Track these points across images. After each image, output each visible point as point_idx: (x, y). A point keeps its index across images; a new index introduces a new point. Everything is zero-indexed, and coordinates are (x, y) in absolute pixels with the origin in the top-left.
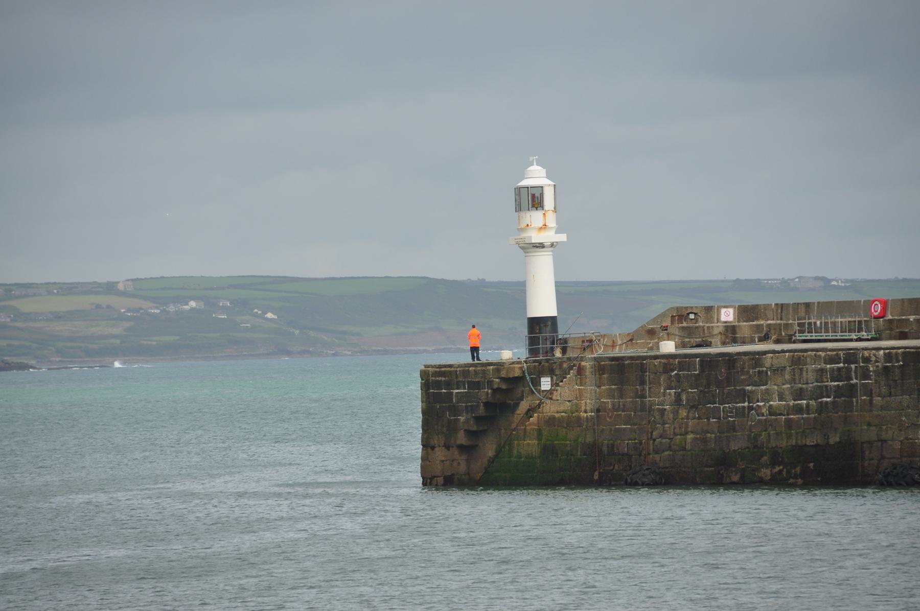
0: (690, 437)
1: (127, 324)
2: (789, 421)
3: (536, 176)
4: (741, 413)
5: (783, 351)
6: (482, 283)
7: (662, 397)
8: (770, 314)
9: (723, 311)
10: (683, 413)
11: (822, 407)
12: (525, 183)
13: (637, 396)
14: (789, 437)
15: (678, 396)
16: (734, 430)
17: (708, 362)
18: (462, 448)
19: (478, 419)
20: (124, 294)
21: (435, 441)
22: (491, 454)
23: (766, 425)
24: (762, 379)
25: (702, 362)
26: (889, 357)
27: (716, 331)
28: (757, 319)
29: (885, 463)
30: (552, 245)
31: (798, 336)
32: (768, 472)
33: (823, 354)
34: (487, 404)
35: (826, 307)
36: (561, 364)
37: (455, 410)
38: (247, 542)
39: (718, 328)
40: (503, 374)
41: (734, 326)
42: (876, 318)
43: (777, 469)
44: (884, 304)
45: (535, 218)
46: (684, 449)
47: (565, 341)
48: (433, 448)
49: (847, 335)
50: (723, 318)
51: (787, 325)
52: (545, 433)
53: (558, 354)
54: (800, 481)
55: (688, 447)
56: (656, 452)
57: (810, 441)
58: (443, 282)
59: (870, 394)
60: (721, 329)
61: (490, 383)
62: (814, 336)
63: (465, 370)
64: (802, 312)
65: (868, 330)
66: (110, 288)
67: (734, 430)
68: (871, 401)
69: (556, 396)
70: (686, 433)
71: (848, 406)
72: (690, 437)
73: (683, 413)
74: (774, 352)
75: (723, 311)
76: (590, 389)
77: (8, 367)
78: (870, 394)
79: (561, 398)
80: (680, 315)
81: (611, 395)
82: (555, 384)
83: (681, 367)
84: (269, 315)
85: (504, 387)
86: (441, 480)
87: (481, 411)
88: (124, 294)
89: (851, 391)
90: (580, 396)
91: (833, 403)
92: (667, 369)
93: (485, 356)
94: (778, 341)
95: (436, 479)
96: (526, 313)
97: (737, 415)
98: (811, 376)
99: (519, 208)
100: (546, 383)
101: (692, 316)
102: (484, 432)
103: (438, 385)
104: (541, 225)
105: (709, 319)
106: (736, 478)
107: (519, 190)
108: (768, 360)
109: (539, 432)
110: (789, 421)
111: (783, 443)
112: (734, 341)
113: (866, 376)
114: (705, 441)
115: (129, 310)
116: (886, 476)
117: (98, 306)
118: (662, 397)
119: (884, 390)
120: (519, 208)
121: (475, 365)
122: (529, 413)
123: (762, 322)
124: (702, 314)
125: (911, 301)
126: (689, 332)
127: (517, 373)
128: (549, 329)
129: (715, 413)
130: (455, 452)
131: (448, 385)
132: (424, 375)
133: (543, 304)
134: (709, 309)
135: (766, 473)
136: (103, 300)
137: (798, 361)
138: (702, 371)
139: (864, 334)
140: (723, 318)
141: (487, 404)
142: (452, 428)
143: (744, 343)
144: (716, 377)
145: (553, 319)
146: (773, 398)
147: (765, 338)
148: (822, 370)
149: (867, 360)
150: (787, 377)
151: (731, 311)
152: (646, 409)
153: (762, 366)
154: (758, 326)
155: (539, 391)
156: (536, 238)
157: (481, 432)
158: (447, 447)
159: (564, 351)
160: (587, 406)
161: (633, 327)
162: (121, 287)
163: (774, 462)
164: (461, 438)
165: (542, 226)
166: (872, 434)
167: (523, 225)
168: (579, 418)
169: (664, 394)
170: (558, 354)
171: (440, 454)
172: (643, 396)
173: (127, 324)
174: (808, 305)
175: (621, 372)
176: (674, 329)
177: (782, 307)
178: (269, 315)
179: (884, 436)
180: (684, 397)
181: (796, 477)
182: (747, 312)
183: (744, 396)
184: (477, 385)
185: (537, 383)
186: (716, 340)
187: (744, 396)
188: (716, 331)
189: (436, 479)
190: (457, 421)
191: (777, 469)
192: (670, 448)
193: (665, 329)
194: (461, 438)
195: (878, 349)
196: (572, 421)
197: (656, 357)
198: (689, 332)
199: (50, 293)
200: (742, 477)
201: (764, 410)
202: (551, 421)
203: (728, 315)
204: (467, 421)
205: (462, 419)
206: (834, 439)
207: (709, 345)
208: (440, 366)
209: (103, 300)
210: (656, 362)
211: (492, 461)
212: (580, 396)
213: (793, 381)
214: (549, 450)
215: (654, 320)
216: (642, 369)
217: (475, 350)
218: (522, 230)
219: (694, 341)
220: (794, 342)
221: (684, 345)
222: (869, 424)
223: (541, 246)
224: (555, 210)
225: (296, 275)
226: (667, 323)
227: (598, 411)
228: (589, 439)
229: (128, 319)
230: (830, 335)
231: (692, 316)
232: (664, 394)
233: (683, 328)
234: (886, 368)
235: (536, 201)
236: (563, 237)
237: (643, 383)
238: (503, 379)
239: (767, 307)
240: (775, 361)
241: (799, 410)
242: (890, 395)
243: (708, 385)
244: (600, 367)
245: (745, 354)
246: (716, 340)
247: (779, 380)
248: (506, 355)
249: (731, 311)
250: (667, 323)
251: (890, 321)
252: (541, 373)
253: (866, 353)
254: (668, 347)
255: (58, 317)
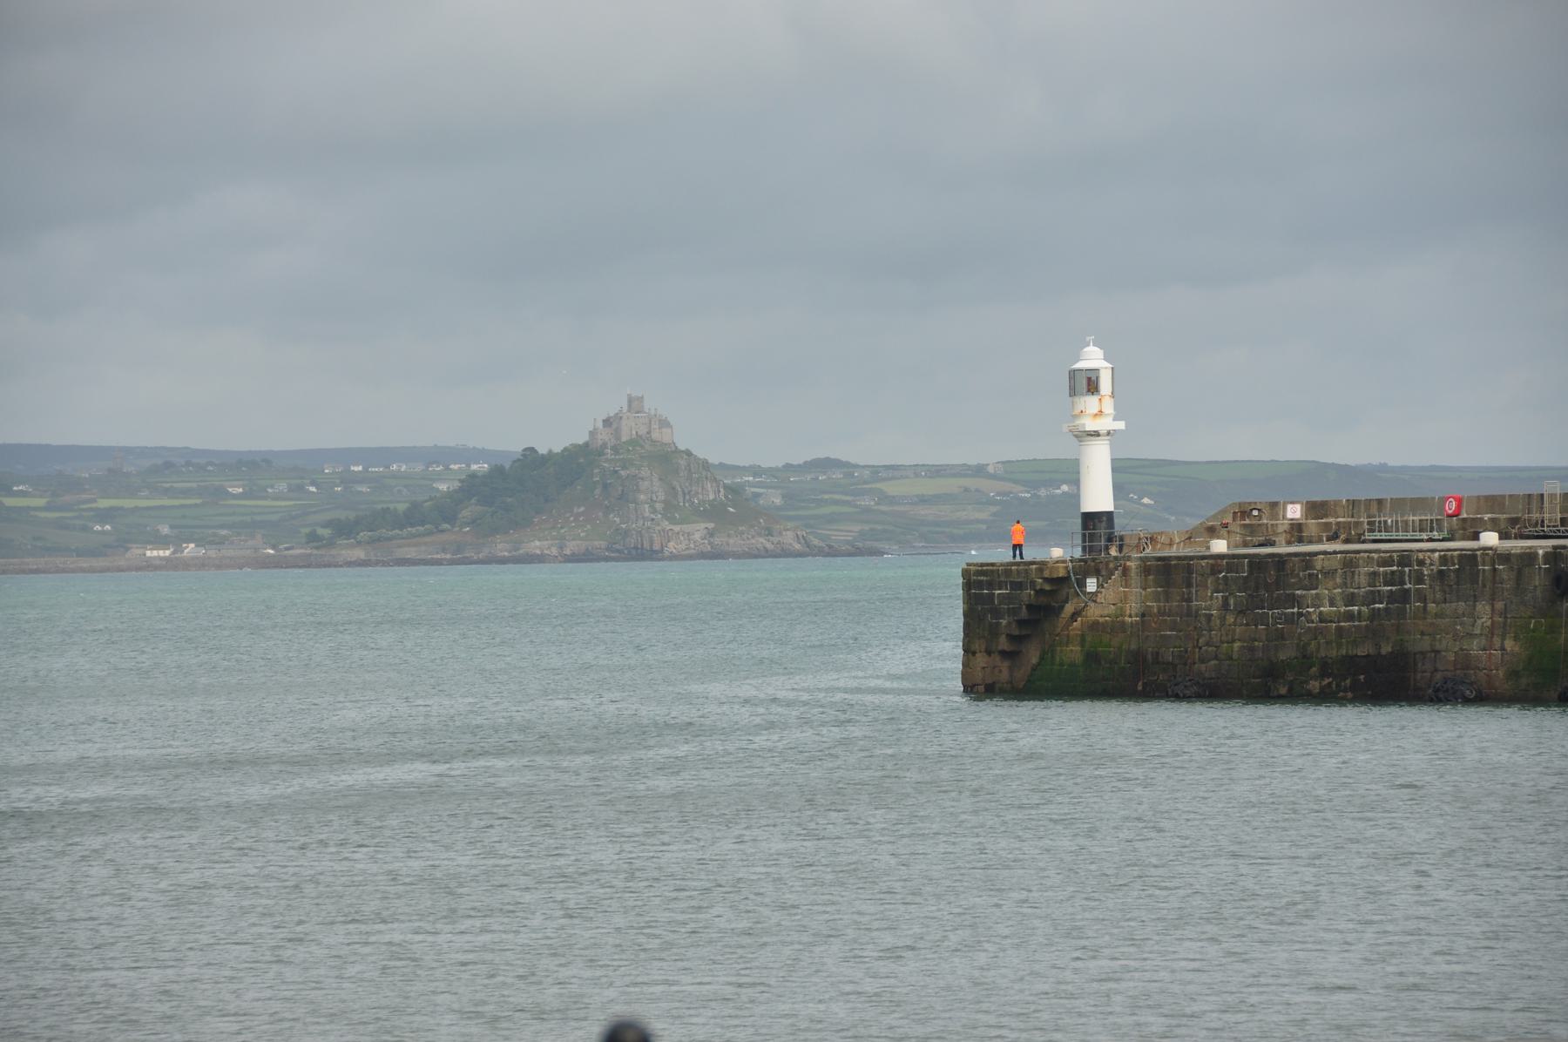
0: (1237, 645)
1: (994, 509)
2: (1339, 629)
3: (1092, 358)
4: (1290, 620)
5: (1335, 552)
6: (1383, 468)
7: (1209, 601)
8: (1340, 511)
9: (1290, 507)
10: (1230, 619)
11: (1375, 614)
12: (1079, 365)
13: (1183, 600)
14: (1339, 646)
15: (1225, 599)
16: (1283, 638)
17: (1257, 563)
18: (1003, 654)
19: (1021, 623)
20: (994, 477)
21: (976, 646)
22: (1034, 661)
23: (1316, 633)
24: (1313, 582)
25: (1251, 564)
26: (1444, 560)
27: (1280, 530)
28: (1326, 516)
29: (1439, 676)
30: (1109, 433)
31: (1368, 536)
32: (1317, 684)
33: (1375, 556)
34: (1029, 607)
35: (1399, 504)
36: (1107, 564)
37: (997, 613)
38: (54, 794)
39: (1283, 526)
40: (1046, 574)
41: (1300, 525)
42: (1450, 516)
43: (1326, 681)
44: (1459, 501)
45: (1090, 403)
46: (1231, 658)
47: (1121, 538)
48: (974, 653)
49: (1418, 535)
50: (1290, 515)
51: (1357, 524)
52: (1089, 639)
53: (1113, 552)
54: (1350, 695)
55: (1235, 656)
56: (1202, 661)
57: (1361, 652)
58: (1334, 466)
59: (1424, 600)
60: (1286, 527)
61: (1033, 583)
62: (1384, 536)
63: (1007, 569)
64: (1374, 510)
65: (1440, 530)
66: (979, 471)
67: (1283, 638)
68: (1425, 608)
69: (1100, 599)
70: (1233, 641)
71: (1401, 614)
72: (1237, 645)
73: (1230, 619)
74: (1325, 553)
75: (1290, 507)
76: (1135, 591)
77: (4, 572)
78: (1424, 600)
79: (1107, 600)
80: (1243, 512)
81: (1157, 598)
82: (1100, 586)
83: (1230, 569)
84: (1146, 500)
85: (1047, 587)
86: (981, 688)
87: (1024, 614)
88: (994, 477)
89: (1404, 596)
90: (1125, 598)
91: (1386, 609)
92: (1214, 570)
93: (1030, 554)
94: (1347, 541)
95: (979, 687)
96: (1078, 505)
97: (1286, 622)
98: (1363, 580)
99: (1073, 392)
100: (1091, 585)
101: (1255, 513)
102: (1027, 637)
103: (980, 585)
104: (1096, 411)
105: (1274, 516)
106: (1283, 691)
107: (1073, 374)
108: (1319, 562)
109: (1083, 637)
110: (1339, 629)
111: (1334, 653)
112: (1300, 540)
113: (1420, 580)
114: (1252, 649)
115: (998, 494)
116: (1437, 690)
117: (966, 490)
118: (1209, 601)
119: (1439, 596)
120: (1073, 392)
121: (1018, 564)
122: (1074, 617)
123: (1331, 520)
124: (1266, 511)
125: (1487, 498)
126: (1252, 529)
127: (1062, 573)
128: (1104, 524)
129: (1263, 619)
130: (997, 658)
131: (990, 585)
132: (966, 574)
133: (1098, 496)
134: (1274, 505)
135: (1314, 686)
136: (971, 483)
137: (1350, 563)
138: (1251, 572)
139: (1435, 534)
140: (1290, 515)
141: (1029, 607)
142: (994, 631)
143: (1310, 542)
144: (1266, 579)
145: (1109, 515)
146: (1323, 603)
147: (1333, 538)
148: (1375, 574)
149: (1421, 563)
150: (1338, 580)
151: (1298, 507)
152: (1191, 614)
153: (1313, 568)
154: (1327, 524)
155: (1085, 593)
156: (1090, 425)
157: (1025, 638)
158: (989, 653)
159: (1121, 548)
160: (1133, 607)
161: (1193, 522)
162: (991, 470)
163: (1324, 674)
164: (1003, 643)
165: (1098, 413)
166: (1425, 644)
167: (1077, 411)
168: (1123, 622)
169: (1211, 598)
170: (1113, 552)
171: (981, 660)
172: (1189, 600)
173: (994, 509)
174: (1380, 502)
175: (1169, 573)
176: (1236, 527)
177: (1353, 503)
178: (1146, 500)
179: (1438, 647)
180: (1232, 602)
181: (1345, 691)
182: (1316, 509)
183: (1293, 600)
184: (1018, 586)
185: (1082, 585)
186: (1281, 539)
187: (1293, 600)
188: (1280, 530)
189: (979, 687)
190: (998, 624)
191: (1326, 681)
192: (1216, 658)
193: (1225, 526)
194: (1003, 643)
195: (1433, 551)
196: (1116, 626)
197: (1203, 558)
198: (1252, 529)
199: (917, 475)
200: (1290, 690)
201: (1314, 617)
202: (1095, 626)
203: (1294, 512)
204: (1009, 624)
205: (1004, 622)
206: (1386, 649)
207: (1272, 544)
208: (982, 565)
209: (971, 483)
210: (1204, 563)
211: (1034, 669)
212: (1125, 598)
213: (1345, 585)
214: (1092, 657)
215: (1214, 517)
216: (1189, 570)
217: (1017, 547)
218: (1075, 417)
219: (1256, 540)
220: (1364, 542)
221: (1245, 545)
222: (1423, 634)
223: (1096, 434)
224: (1113, 395)
225: (1169, 457)
226: (1228, 519)
227: (1143, 615)
228: (1133, 647)
229: (992, 502)
230: (1401, 535)
231: (1255, 513)
232: (1211, 598)
233: (1245, 526)
234: (1441, 572)
235: (1092, 387)
236: (1121, 425)
237: (1189, 585)
238: (1046, 580)
239: (1337, 503)
240: (1326, 563)
241: (1350, 616)
242: (1445, 601)
243: (1257, 588)
244: (1146, 569)
245: (1296, 555)
246: (1281, 539)
247: (1330, 584)
248: (1057, 553)
249: (1298, 507)
250: (1228, 519)
251: (1464, 520)
252: (1087, 574)
253: (1421, 556)
254: (1220, 546)
255: (923, 500)
